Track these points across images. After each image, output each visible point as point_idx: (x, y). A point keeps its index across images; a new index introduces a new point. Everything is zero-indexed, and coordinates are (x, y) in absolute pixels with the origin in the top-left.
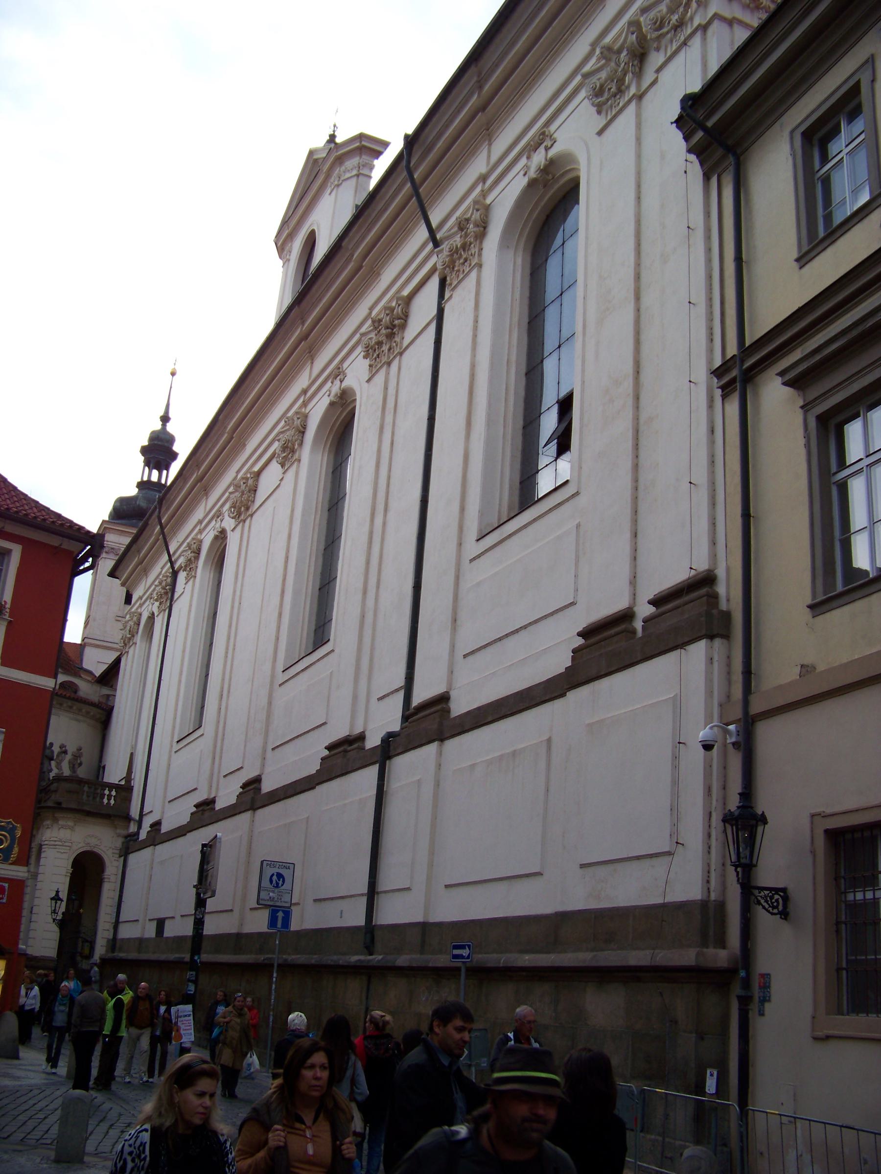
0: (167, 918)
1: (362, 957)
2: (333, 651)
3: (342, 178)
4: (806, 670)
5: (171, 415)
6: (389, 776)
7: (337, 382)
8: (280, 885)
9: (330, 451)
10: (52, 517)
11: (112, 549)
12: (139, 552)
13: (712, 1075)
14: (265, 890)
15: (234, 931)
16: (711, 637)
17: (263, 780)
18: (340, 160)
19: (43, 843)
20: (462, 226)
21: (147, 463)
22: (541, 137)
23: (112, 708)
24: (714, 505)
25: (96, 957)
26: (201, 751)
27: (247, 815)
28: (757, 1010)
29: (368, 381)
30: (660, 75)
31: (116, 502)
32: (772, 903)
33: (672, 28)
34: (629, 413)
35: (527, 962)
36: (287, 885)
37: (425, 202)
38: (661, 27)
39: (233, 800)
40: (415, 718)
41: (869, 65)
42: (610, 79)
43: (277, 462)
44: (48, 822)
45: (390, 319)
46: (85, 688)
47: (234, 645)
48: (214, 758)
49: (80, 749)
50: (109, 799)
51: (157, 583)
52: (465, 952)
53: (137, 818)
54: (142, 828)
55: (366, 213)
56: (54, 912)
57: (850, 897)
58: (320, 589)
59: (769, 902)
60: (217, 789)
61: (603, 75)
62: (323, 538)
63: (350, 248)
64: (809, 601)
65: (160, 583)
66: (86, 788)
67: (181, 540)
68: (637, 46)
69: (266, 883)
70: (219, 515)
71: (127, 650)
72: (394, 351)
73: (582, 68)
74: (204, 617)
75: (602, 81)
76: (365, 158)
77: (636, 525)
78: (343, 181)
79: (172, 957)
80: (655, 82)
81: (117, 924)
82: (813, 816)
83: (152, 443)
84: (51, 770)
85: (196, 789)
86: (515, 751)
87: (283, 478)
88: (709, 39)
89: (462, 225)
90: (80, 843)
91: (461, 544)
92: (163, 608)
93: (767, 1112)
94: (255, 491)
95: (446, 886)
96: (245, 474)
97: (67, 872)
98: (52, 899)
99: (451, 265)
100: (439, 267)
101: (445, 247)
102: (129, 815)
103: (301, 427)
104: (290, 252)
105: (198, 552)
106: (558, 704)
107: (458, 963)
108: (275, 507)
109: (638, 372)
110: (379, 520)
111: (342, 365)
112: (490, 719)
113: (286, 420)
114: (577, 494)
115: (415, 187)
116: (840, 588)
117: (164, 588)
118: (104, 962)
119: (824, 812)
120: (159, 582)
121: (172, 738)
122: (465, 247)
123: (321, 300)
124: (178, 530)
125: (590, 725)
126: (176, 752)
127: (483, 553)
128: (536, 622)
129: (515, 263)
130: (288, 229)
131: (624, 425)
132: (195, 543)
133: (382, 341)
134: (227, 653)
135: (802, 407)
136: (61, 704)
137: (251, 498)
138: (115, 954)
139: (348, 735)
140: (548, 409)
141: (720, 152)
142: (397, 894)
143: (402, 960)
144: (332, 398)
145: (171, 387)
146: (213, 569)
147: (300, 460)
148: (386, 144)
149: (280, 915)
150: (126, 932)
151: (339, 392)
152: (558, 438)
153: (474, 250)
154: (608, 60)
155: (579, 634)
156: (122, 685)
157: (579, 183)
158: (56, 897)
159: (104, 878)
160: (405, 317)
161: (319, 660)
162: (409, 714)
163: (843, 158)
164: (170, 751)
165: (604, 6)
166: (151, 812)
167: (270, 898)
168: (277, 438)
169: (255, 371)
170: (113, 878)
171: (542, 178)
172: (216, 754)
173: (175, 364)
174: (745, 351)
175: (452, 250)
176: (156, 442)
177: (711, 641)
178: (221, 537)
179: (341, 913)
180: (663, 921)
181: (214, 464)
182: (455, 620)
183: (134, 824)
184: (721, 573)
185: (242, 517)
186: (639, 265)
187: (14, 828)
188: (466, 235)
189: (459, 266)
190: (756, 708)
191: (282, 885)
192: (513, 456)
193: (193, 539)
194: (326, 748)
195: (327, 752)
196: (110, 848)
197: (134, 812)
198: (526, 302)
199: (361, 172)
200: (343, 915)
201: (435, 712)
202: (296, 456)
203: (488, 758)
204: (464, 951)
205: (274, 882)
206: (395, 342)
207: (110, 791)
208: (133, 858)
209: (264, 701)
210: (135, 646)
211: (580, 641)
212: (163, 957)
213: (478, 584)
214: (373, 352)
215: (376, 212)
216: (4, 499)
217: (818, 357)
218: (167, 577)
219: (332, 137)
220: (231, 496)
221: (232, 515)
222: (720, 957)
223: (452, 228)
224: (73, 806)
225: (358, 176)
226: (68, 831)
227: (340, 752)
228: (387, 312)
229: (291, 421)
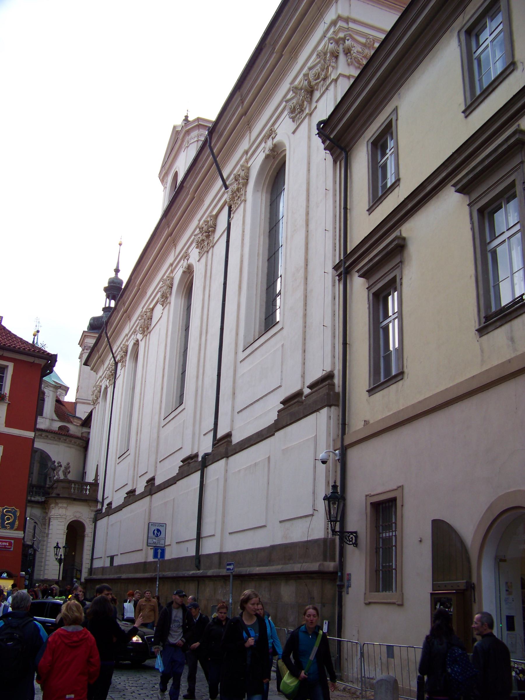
2: (184, 409)
3: (189, 143)
4: (366, 422)
5: (120, 268)
7: (186, 260)
8: (159, 535)
9: (185, 297)
10: (30, 346)
12: (98, 351)
13: (326, 623)
15: (143, 561)
16: (330, 406)
18: (188, 132)
19: (51, 517)
20: (236, 179)
21: (108, 297)
22: (270, 132)
24: (335, 337)
27: (148, 498)
28: (346, 591)
29: (199, 261)
31: (91, 319)
32: (349, 539)
33: (322, 80)
34: (302, 287)
36: (162, 535)
38: (318, 78)
39: (142, 490)
41: (395, 112)
42: (297, 103)
44: (53, 505)
45: (207, 227)
46: (74, 429)
47: (143, 405)
49: (68, 464)
50: (86, 491)
52: (231, 567)
56: (56, 554)
57: (384, 535)
58: (182, 374)
59: (348, 539)
61: (294, 101)
64: (368, 389)
66: (73, 485)
67: (118, 345)
68: (309, 87)
69: (151, 534)
70: (186, 256)
71: (95, 407)
73: (287, 96)
75: (294, 104)
77: (305, 346)
78: (190, 144)
79: (116, 576)
80: (316, 108)
81: (92, 559)
82: (366, 496)
83: (110, 285)
84: (55, 476)
85: (127, 484)
86: (255, 463)
87: (163, 313)
88: (338, 86)
90: (71, 516)
93: (374, 644)
94: (151, 319)
95: (230, 533)
96: (146, 309)
97: (64, 532)
98: (55, 547)
99: (232, 198)
100: (228, 200)
101: (229, 190)
102: (97, 499)
103: (170, 284)
106: (272, 438)
107: (229, 572)
109: (307, 265)
111: (188, 251)
113: (163, 281)
114: (282, 328)
115: (215, 158)
116: (382, 380)
117: (111, 372)
119: (370, 494)
122: (238, 190)
123: (176, 214)
125: (283, 450)
126: (118, 464)
129: (262, 200)
130: (165, 170)
131: (300, 294)
132: (124, 347)
133: (204, 239)
135: (367, 288)
136: (60, 439)
137: (149, 323)
141: (339, 151)
142: (209, 538)
143: (210, 573)
144: (184, 269)
145: (119, 252)
149: (159, 551)
150: (97, 564)
151: (187, 266)
153: (242, 192)
154: (296, 94)
158: (57, 547)
159: (85, 535)
162: (216, 442)
163: (388, 157)
164: (115, 463)
166: (108, 497)
167: (154, 542)
168: (160, 290)
169: (147, 254)
171: (271, 154)
172: (135, 465)
174: (347, 256)
177: (330, 408)
178: (189, 271)
179: (187, 549)
180: (307, 549)
184: (336, 373)
185: (145, 334)
186: (308, 207)
187: (16, 511)
188: (239, 183)
189: (236, 200)
190: (347, 442)
191: (160, 535)
192: (261, 305)
197: (100, 498)
198: (268, 220)
199: (199, 139)
201: (225, 442)
202: (168, 301)
205: (156, 534)
206: (210, 240)
210: (99, 404)
211: (282, 406)
212: (112, 576)
213: (243, 374)
214: (200, 244)
216: (3, 339)
217: (371, 264)
218: (112, 365)
219: (187, 117)
221: (140, 332)
222: (331, 566)
224: (66, 495)
226: (64, 510)
228: (206, 224)
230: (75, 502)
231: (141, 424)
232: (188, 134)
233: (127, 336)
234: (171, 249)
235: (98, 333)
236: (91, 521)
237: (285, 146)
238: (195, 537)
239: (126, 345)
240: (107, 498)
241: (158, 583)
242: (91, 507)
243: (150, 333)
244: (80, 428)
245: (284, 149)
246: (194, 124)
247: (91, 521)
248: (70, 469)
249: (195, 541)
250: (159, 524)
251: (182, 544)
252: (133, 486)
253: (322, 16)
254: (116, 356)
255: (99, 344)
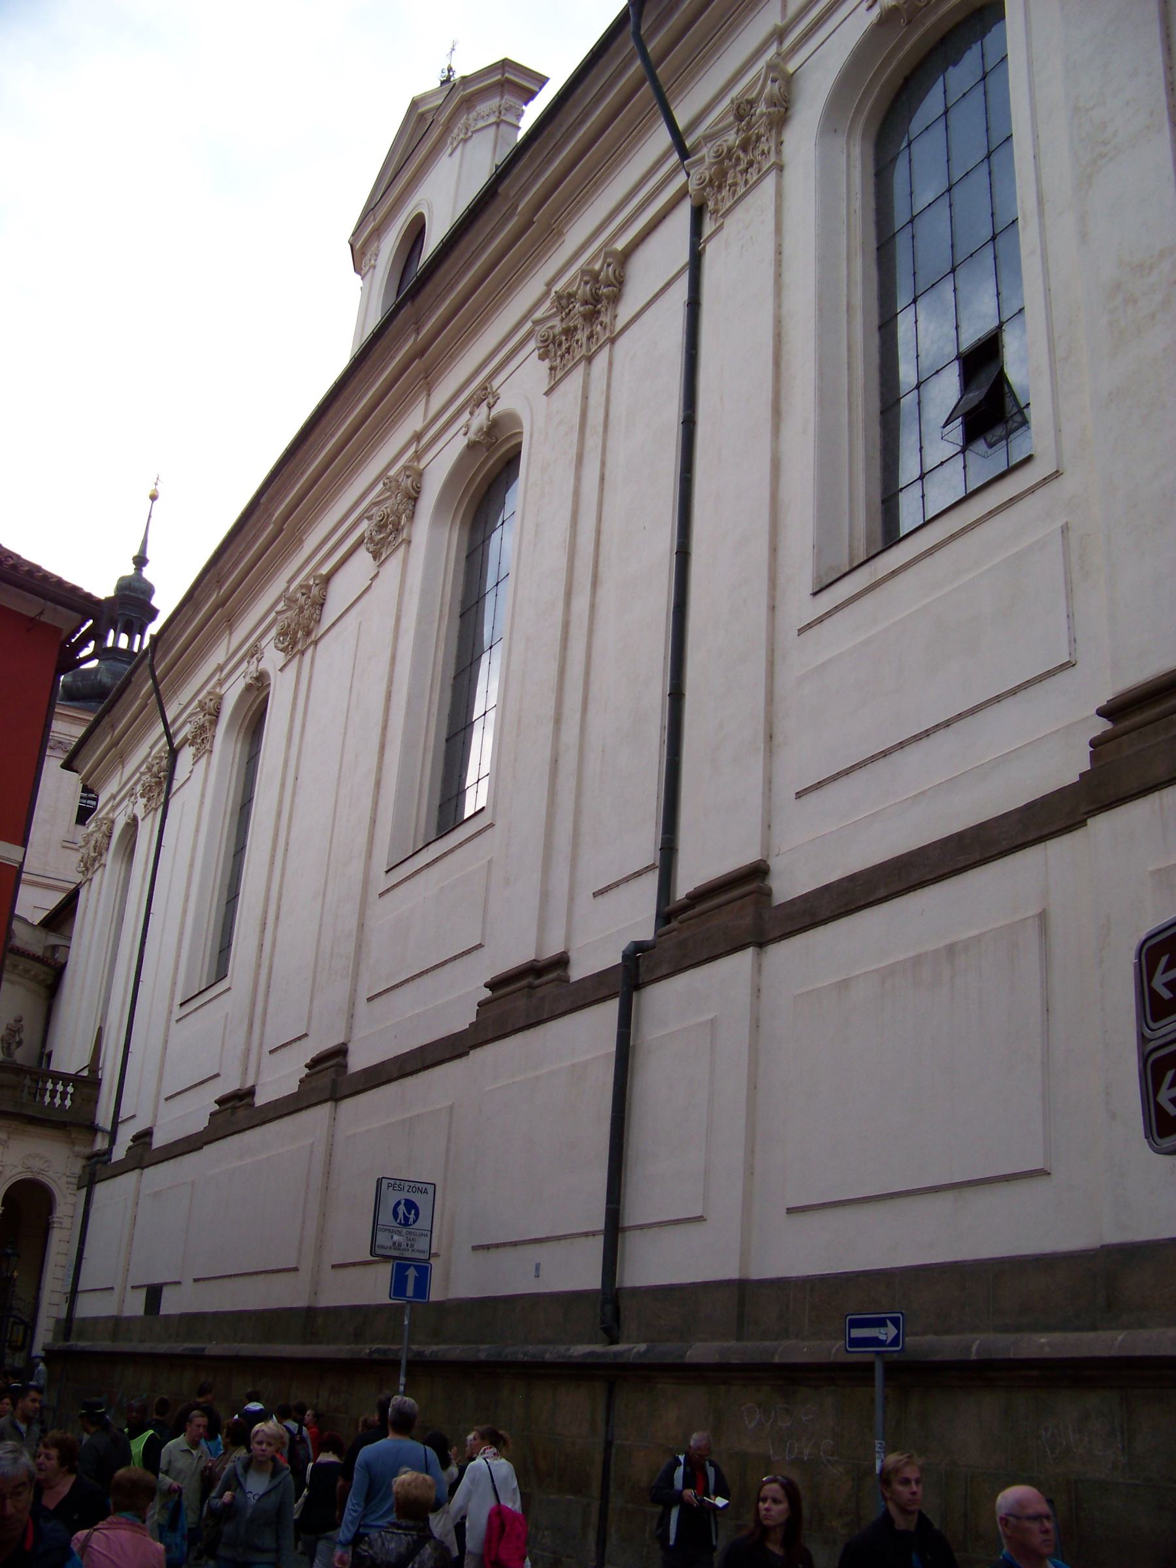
0: (166, 1284)
1: (598, 1348)
2: (491, 825)
3: (472, 129)
5: (149, 556)
6: (637, 1023)
8: (411, 1220)
9: (245, 733)
11: (60, 742)
12: (113, 727)
14: (385, 1230)
17: (350, 1051)
18: (468, 103)
20: (741, 111)
23: (64, 966)
25: (38, 1350)
26: (227, 1015)
30: (381, 570)
35: (1047, 1349)
36: (423, 1223)
37: (665, 90)
39: (292, 1087)
40: (691, 913)
43: (368, 549)
47: (287, 844)
48: (251, 1025)
49: (19, 1020)
50: (53, 1097)
51: (143, 769)
52: (887, 1333)
53: (109, 1128)
54: (117, 1143)
55: (545, 133)
60: (258, 1073)
62: (452, 661)
63: (511, 195)
65: (150, 769)
66: (28, 1081)
67: (185, 702)
69: (386, 1218)
70: (255, 652)
71: (89, 876)
72: (598, 339)
73: (533, 314)
74: (225, 812)
76: (509, 99)
78: (474, 132)
79: (179, 1347)
81: (73, 1294)
85: (217, 1075)
89: (742, 111)
90: (16, 1166)
91: (774, 607)
92: (153, 805)
94: (322, 605)
96: (307, 578)
99: (717, 181)
104: (377, 255)
105: (216, 714)
106: (1077, 836)
108: (360, 623)
110: (581, 603)
112: (882, 893)
115: (650, 68)
117: (156, 776)
118: (51, 1355)
120: (147, 768)
121: (172, 999)
123: (452, 288)
124: (180, 686)
126: (177, 1021)
127: (829, 614)
128: (973, 711)
129: (848, 156)
130: (375, 220)
132: (211, 700)
134: (273, 857)
137: (314, 616)
138: (70, 1343)
139: (534, 960)
140: (937, 372)
146: (242, 735)
147: (410, 542)
148: (542, 80)
149: (412, 1273)
150: (88, 1308)
152: (966, 416)
155: (486, 986)
156: (82, 929)
157: (520, 452)
159: (53, 1222)
160: (619, 282)
161: (461, 845)
162: (667, 914)
164: (169, 1021)
165: (563, 242)
167: (394, 1244)
168: (366, 515)
170: (67, 1223)
171: (906, 6)
173: (156, 484)
175: (721, 154)
176: (127, 593)
178: (259, 686)
181: (246, 577)
182: (770, 737)
183: (103, 1139)
185: (299, 647)
188: (749, 126)
191: (415, 1221)
193: (209, 693)
194: (216, 1102)
195: (487, 993)
196: (65, 1174)
197: (104, 1118)
198: (872, 217)
199: (503, 118)
200: (541, 1273)
202: (404, 535)
203: (882, 965)
204: (882, 1330)
205: (401, 1216)
207: (65, 1086)
208: (101, 1190)
209: (353, 923)
212: (163, 1348)
215: (564, 129)
218: (161, 758)
220: (279, 617)
221: (281, 646)
223: (722, 119)
225: (498, 124)
227: (520, 990)
229: (394, 484)
230: (31, 1128)
231: (280, 898)
232: (468, 109)
233: (115, 799)
234: (223, 633)
235: (94, 712)
236: (71, 1183)
237: (521, 426)
238: (600, 1224)
239: (216, 695)
240: (132, 1121)
241: (402, 1380)
242: (74, 1144)
243: (316, 645)
244: (41, 934)
245: (517, 431)
246: (491, 77)
247: (71, 1183)
248: (22, 1035)
249: (600, 1241)
250: (412, 1184)
251: (494, 1254)
252: (244, 1080)
253: (176, 693)
254: (176, 733)
255: (118, 706)
